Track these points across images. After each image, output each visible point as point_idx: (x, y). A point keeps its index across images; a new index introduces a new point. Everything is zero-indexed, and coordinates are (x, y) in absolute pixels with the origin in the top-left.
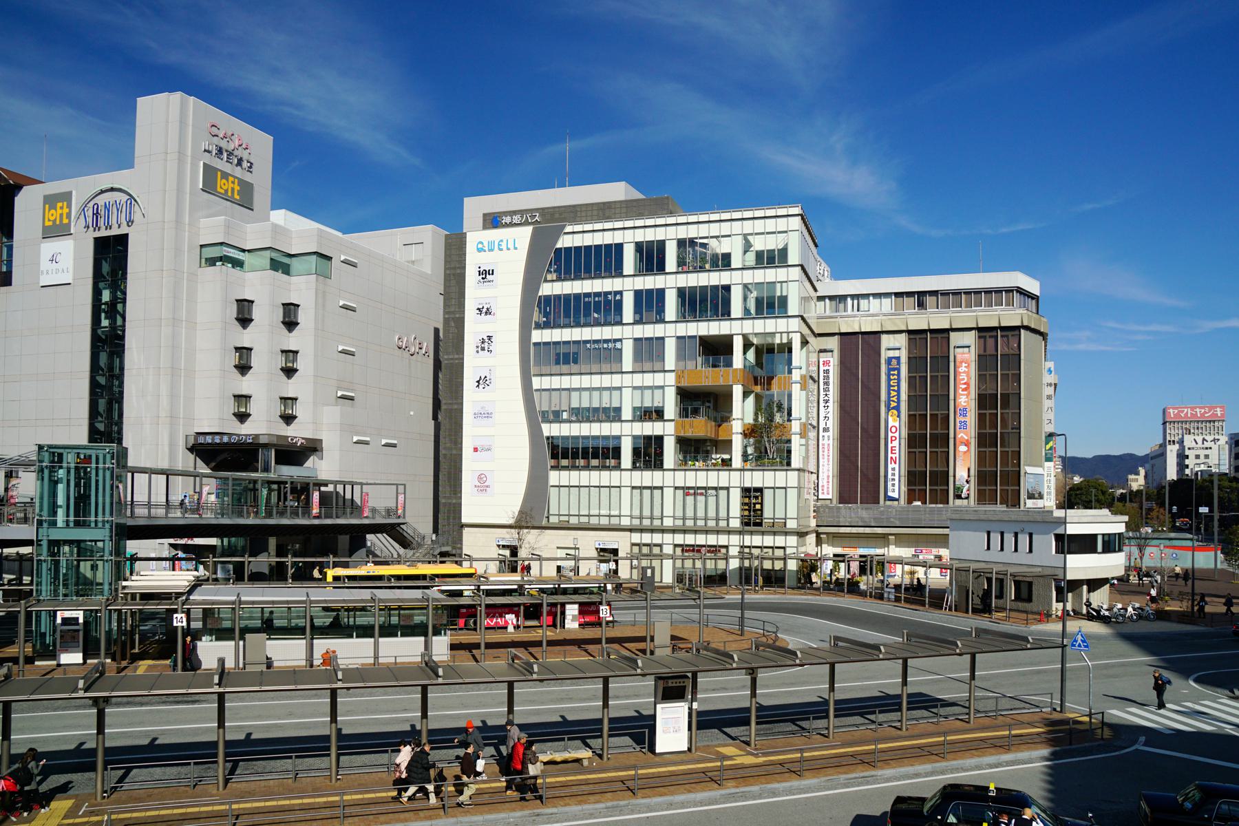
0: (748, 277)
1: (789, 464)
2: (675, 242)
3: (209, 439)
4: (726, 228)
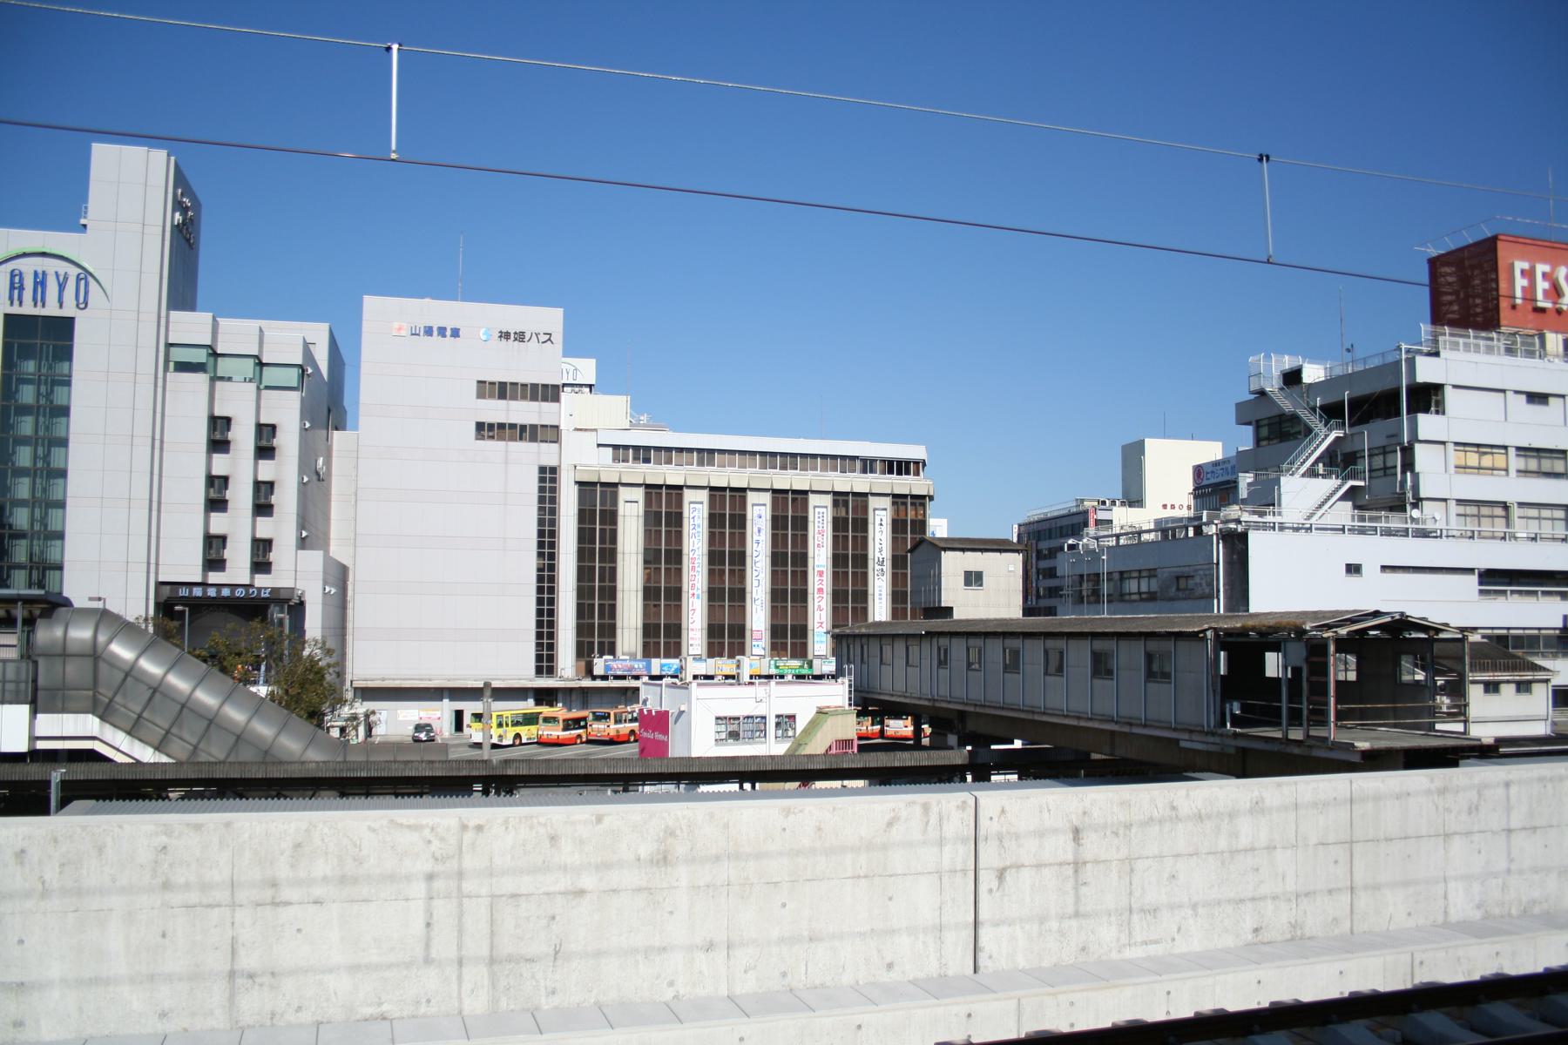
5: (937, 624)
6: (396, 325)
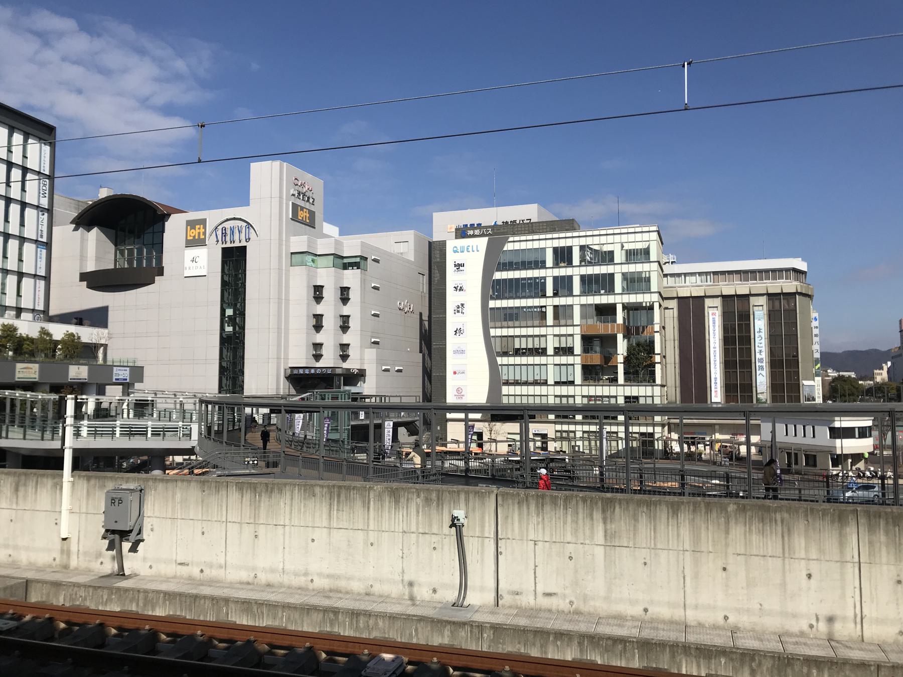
0: (626, 268)
1: (654, 381)
2: (578, 248)
3: (301, 371)
4: (610, 239)
6: (449, 226)
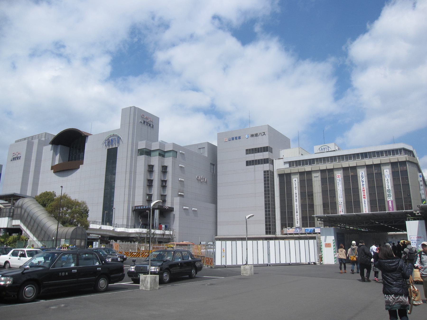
3: (139, 208)
5: (238, 277)
